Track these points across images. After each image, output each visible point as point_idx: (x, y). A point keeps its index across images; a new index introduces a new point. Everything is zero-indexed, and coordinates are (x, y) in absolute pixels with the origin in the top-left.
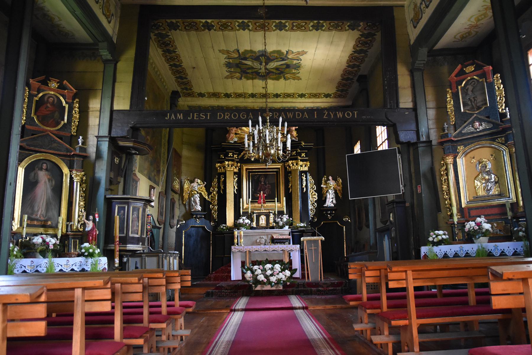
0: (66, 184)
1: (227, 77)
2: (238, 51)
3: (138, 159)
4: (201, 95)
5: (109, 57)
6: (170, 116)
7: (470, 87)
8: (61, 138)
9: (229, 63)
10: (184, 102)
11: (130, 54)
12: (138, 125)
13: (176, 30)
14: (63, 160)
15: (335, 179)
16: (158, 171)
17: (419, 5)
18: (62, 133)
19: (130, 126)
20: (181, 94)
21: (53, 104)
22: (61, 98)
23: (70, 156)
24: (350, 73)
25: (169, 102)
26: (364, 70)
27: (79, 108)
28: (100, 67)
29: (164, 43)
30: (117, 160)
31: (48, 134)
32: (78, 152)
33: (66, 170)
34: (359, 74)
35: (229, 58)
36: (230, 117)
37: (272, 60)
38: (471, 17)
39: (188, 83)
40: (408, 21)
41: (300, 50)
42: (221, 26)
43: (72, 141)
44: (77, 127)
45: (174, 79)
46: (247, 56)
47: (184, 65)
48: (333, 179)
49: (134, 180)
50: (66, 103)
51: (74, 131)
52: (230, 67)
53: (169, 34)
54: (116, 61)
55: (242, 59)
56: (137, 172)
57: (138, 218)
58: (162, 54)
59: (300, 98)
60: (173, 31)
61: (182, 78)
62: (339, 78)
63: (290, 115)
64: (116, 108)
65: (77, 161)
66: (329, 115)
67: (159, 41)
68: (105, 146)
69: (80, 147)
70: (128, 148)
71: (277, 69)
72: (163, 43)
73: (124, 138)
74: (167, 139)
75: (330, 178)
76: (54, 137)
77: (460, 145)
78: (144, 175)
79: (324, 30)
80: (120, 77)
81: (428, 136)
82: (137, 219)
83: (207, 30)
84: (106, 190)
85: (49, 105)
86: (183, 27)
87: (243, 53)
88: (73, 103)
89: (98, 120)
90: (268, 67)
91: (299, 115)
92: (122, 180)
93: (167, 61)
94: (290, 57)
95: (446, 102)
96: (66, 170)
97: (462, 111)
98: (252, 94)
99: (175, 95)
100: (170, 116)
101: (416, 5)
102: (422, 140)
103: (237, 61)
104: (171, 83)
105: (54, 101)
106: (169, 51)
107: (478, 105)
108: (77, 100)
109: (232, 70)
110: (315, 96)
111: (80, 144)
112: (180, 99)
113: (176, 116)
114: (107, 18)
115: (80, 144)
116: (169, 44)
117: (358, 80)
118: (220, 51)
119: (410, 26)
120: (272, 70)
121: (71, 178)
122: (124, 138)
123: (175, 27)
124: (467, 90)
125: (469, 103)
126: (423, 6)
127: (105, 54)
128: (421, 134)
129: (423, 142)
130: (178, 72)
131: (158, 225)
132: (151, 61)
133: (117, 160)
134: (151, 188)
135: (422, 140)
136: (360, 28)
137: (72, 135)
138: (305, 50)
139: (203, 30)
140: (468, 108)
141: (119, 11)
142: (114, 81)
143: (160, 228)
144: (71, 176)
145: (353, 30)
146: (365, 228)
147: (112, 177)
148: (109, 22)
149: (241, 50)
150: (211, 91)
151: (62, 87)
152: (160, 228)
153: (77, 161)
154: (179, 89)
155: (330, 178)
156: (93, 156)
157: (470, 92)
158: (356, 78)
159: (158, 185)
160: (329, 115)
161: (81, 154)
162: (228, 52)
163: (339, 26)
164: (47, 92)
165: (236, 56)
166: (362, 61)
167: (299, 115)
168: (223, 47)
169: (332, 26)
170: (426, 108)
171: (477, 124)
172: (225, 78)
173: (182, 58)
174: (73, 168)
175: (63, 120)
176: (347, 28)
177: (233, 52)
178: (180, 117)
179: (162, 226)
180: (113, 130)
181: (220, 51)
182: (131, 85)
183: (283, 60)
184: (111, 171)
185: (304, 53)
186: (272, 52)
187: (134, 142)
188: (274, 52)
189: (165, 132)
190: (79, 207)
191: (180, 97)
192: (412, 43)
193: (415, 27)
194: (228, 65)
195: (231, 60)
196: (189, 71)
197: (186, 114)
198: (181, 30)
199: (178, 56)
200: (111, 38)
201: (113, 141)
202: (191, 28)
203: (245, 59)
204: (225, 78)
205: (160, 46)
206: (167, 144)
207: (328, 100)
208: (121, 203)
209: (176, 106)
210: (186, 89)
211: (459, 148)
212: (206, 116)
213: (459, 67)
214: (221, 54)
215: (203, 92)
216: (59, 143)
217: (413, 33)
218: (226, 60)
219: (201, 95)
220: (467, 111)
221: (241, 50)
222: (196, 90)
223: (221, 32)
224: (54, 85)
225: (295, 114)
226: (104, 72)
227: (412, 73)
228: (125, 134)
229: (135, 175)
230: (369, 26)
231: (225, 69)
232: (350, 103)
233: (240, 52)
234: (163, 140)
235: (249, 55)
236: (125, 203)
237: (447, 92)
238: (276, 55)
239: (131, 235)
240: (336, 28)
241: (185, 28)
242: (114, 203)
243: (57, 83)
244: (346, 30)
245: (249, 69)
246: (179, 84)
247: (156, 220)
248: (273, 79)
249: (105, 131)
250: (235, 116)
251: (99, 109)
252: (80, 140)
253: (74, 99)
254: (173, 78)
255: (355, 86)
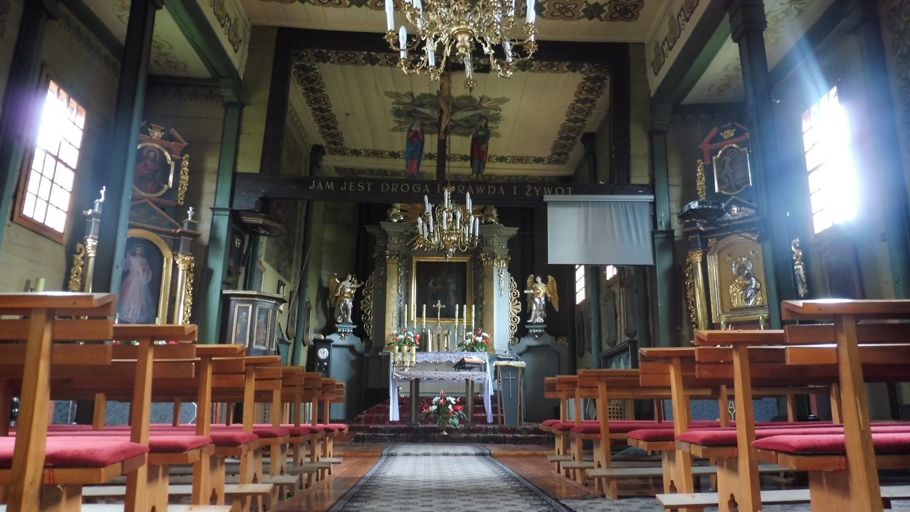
0: (167, 274)
1: (394, 130)
2: (412, 94)
3: (264, 241)
4: (356, 153)
5: (234, 100)
6: (316, 185)
7: (728, 159)
8: (163, 209)
9: (399, 110)
10: (330, 162)
11: (263, 95)
12: (271, 196)
13: (325, 62)
14: (165, 239)
15: (545, 281)
16: (291, 262)
17: (660, 44)
18: (164, 202)
19: (260, 195)
20: (326, 150)
21: (154, 161)
22: (166, 153)
23: (175, 234)
24: (571, 130)
25: (308, 159)
26: (591, 125)
27: (188, 167)
28: (219, 112)
29: (307, 79)
30: (238, 243)
31: (147, 203)
32: (185, 228)
33: (167, 254)
34: (585, 130)
35: (398, 103)
36: (399, 189)
37: (460, 109)
38: (728, 66)
39: (338, 135)
40: (648, 64)
41: (499, 96)
42: (390, 59)
43: (179, 213)
44: (186, 193)
45: (317, 128)
46: (425, 102)
47: (333, 110)
48: (542, 281)
49: (259, 271)
50: (173, 159)
51: (181, 200)
52: (399, 116)
53: (316, 67)
54: (241, 105)
55: (416, 106)
56: (262, 259)
57: (266, 322)
58: (304, 93)
59: (498, 163)
60: (321, 63)
61: (329, 127)
62: (555, 137)
63: (480, 190)
64: (240, 169)
65: (184, 242)
66: (533, 191)
67: (300, 75)
68: (223, 223)
69: (189, 223)
70: (256, 226)
71: (466, 120)
72: (306, 79)
73: (250, 212)
74: (304, 215)
75: (539, 279)
76: (154, 207)
77: (712, 238)
78: (271, 265)
79: (533, 71)
80: (246, 126)
81: (669, 225)
82: (264, 325)
83: (369, 65)
84: (223, 283)
85: (148, 162)
86: (336, 59)
87: (418, 97)
88: (181, 160)
89: (214, 185)
90: (453, 117)
91: (492, 190)
92: (243, 269)
93: (310, 103)
94: (485, 105)
95: (696, 178)
96: (167, 254)
97: (717, 190)
98: (430, 154)
99: (318, 151)
100: (316, 185)
101: (657, 44)
102: (659, 228)
103: (410, 108)
104: (314, 135)
105: (155, 156)
106: (313, 90)
107: (737, 183)
108: (187, 156)
109: (403, 120)
110: (520, 160)
111: (190, 218)
112: (324, 157)
113: (324, 185)
114: (233, 46)
115: (190, 218)
116: (314, 81)
117: (583, 140)
118: (386, 93)
119: (650, 72)
120: (460, 123)
121: (175, 266)
122: (250, 212)
123: (325, 59)
124: (724, 162)
125: (726, 180)
126: (666, 47)
127: (228, 94)
128: (659, 220)
129: (662, 232)
130: (323, 118)
131: (286, 339)
132: (289, 109)
133: (238, 243)
134: (280, 284)
135: (659, 228)
136: (583, 70)
137: (178, 205)
138: (507, 97)
139: (364, 65)
140: (725, 187)
141: (248, 34)
142: (239, 132)
143: (289, 344)
144: (174, 262)
145: (574, 71)
146: (587, 352)
147: (232, 265)
148: (236, 51)
149: (417, 94)
150: (370, 146)
151: (169, 138)
152: (289, 344)
153: (184, 242)
154: (323, 143)
155: (539, 279)
156: (205, 237)
157: (727, 166)
158: (579, 138)
159: (289, 280)
160: (533, 191)
161: (190, 231)
162: (397, 95)
163: (554, 66)
164: (147, 144)
165: (409, 100)
166: (588, 114)
167: (492, 190)
168: (391, 88)
169: (546, 66)
170: (668, 186)
171: (735, 209)
172: (392, 130)
173: (332, 100)
174: (178, 251)
175: (167, 182)
176: (566, 69)
177: (405, 95)
178: (330, 186)
179: (292, 341)
180: (236, 201)
181: (386, 93)
182: (262, 138)
183: (475, 109)
184: (230, 255)
185: (504, 100)
186: (459, 98)
187: (264, 218)
188: (463, 97)
189: (302, 205)
190: (184, 305)
191: (325, 153)
192: (652, 94)
193: (656, 74)
194: (397, 113)
195: (401, 107)
196: (340, 119)
197: (338, 182)
198: (333, 63)
199: (326, 98)
200: (237, 73)
201: (235, 216)
202: (347, 60)
203: (421, 105)
204: (392, 130)
205: (301, 83)
206: (303, 222)
207: (540, 166)
208: (243, 302)
209: (319, 168)
210: (335, 143)
211: (710, 240)
212: (366, 187)
213: (714, 130)
214: (387, 97)
215: (358, 149)
216: (160, 215)
217: (655, 82)
218: (396, 106)
219: (356, 153)
220: (723, 192)
221: (417, 94)
222: (349, 144)
223: (389, 68)
224: (157, 134)
225: (486, 189)
226: (225, 120)
227: (652, 134)
228: (252, 206)
229: (260, 263)
230: (597, 67)
231: (392, 118)
232: (571, 172)
233: (415, 95)
234: (298, 216)
235: (428, 100)
236: (249, 302)
237: (697, 165)
238: (465, 102)
239: (255, 347)
240: (550, 68)
241: (339, 60)
242: (232, 303)
243: (162, 131)
244: (564, 72)
245: (427, 119)
246: (325, 135)
247: (284, 331)
248: (460, 135)
249: (223, 202)
250: (405, 188)
251: (216, 170)
252: (190, 212)
253: (182, 155)
254: (317, 128)
255: (577, 151)
